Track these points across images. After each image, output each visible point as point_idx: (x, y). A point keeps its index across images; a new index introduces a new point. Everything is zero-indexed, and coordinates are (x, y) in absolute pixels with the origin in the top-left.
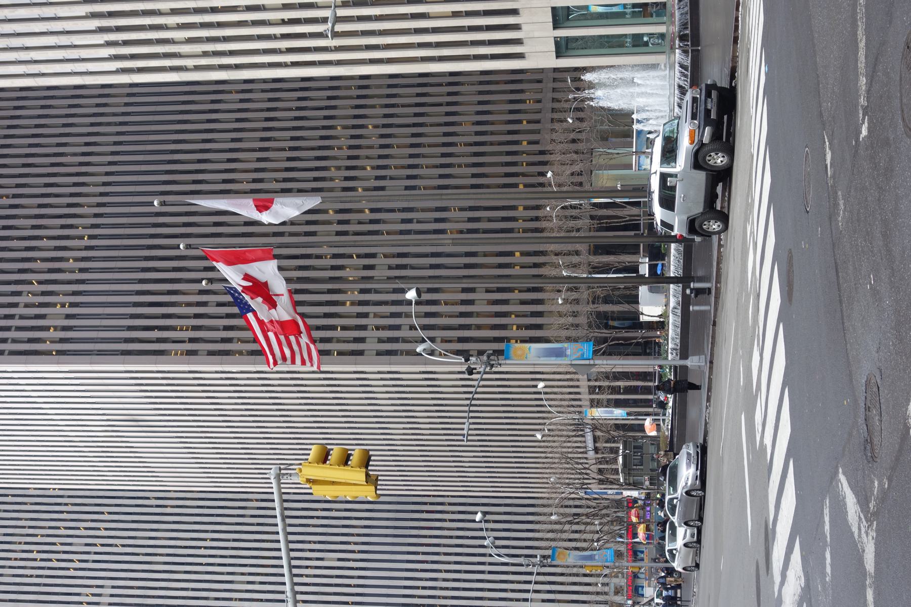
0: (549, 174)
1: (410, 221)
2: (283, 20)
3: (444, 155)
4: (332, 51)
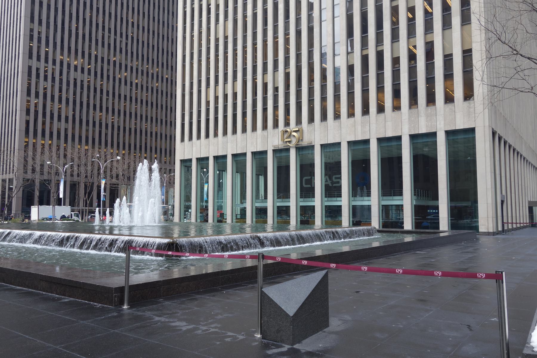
1: (108, 94)
2: (210, 5)
3: (141, 116)
4: (191, 33)
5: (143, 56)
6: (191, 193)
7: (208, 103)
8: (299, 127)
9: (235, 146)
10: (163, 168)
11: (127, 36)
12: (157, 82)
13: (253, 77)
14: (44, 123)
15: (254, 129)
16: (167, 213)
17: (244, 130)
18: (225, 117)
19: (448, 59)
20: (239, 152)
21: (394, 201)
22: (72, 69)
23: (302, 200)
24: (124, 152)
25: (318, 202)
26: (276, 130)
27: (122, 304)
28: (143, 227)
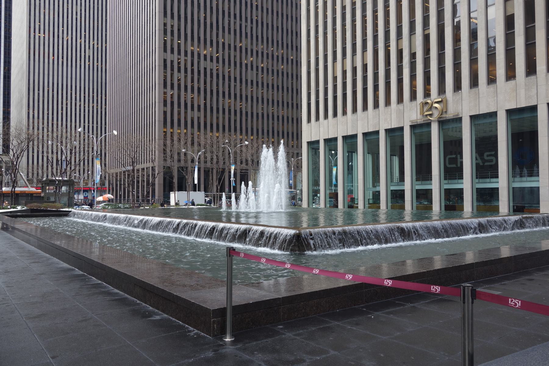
0: (247, 143)
4: (316, 5)
5: (268, 39)
6: (319, 177)
7: (335, 78)
8: (442, 96)
9: (366, 124)
10: (291, 151)
12: (282, 64)
13: (385, 44)
14: (179, 113)
15: (388, 102)
16: (294, 199)
18: (354, 93)
20: (371, 130)
22: (202, 58)
23: (446, 182)
24: (252, 138)
25: (467, 184)
26: (414, 103)
27: (223, 332)
28: (269, 214)
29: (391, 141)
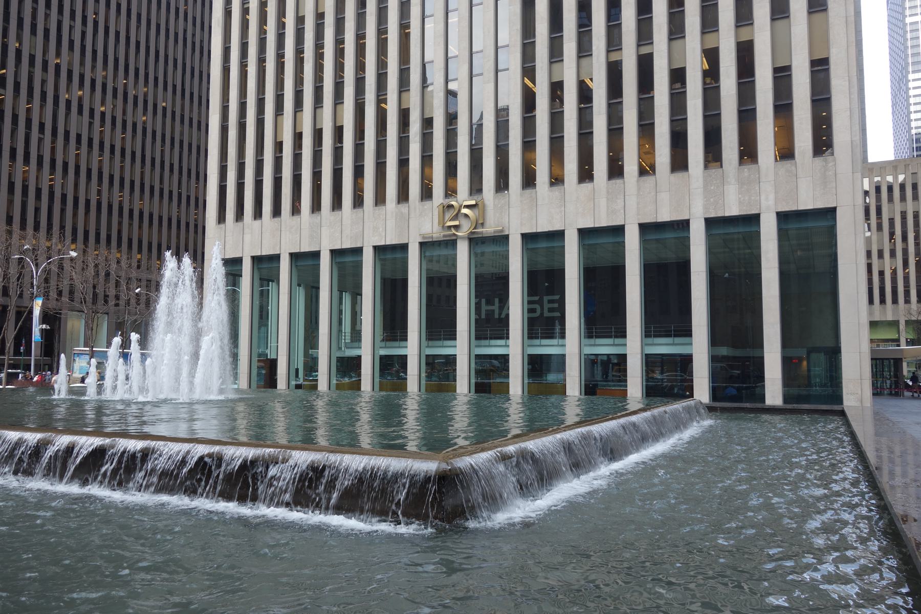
3: (111, 177)
7: (279, 146)
9: (338, 234)
11: (84, 18)
12: (145, 114)
13: (378, 96)
17: (358, 201)
18: (317, 176)
19: (782, 75)
21: (494, 348)
26: (427, 204)
29: (298, 276)
